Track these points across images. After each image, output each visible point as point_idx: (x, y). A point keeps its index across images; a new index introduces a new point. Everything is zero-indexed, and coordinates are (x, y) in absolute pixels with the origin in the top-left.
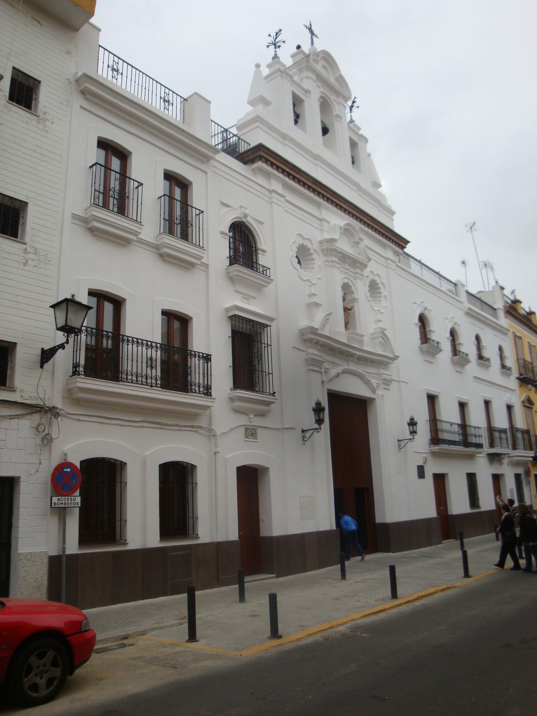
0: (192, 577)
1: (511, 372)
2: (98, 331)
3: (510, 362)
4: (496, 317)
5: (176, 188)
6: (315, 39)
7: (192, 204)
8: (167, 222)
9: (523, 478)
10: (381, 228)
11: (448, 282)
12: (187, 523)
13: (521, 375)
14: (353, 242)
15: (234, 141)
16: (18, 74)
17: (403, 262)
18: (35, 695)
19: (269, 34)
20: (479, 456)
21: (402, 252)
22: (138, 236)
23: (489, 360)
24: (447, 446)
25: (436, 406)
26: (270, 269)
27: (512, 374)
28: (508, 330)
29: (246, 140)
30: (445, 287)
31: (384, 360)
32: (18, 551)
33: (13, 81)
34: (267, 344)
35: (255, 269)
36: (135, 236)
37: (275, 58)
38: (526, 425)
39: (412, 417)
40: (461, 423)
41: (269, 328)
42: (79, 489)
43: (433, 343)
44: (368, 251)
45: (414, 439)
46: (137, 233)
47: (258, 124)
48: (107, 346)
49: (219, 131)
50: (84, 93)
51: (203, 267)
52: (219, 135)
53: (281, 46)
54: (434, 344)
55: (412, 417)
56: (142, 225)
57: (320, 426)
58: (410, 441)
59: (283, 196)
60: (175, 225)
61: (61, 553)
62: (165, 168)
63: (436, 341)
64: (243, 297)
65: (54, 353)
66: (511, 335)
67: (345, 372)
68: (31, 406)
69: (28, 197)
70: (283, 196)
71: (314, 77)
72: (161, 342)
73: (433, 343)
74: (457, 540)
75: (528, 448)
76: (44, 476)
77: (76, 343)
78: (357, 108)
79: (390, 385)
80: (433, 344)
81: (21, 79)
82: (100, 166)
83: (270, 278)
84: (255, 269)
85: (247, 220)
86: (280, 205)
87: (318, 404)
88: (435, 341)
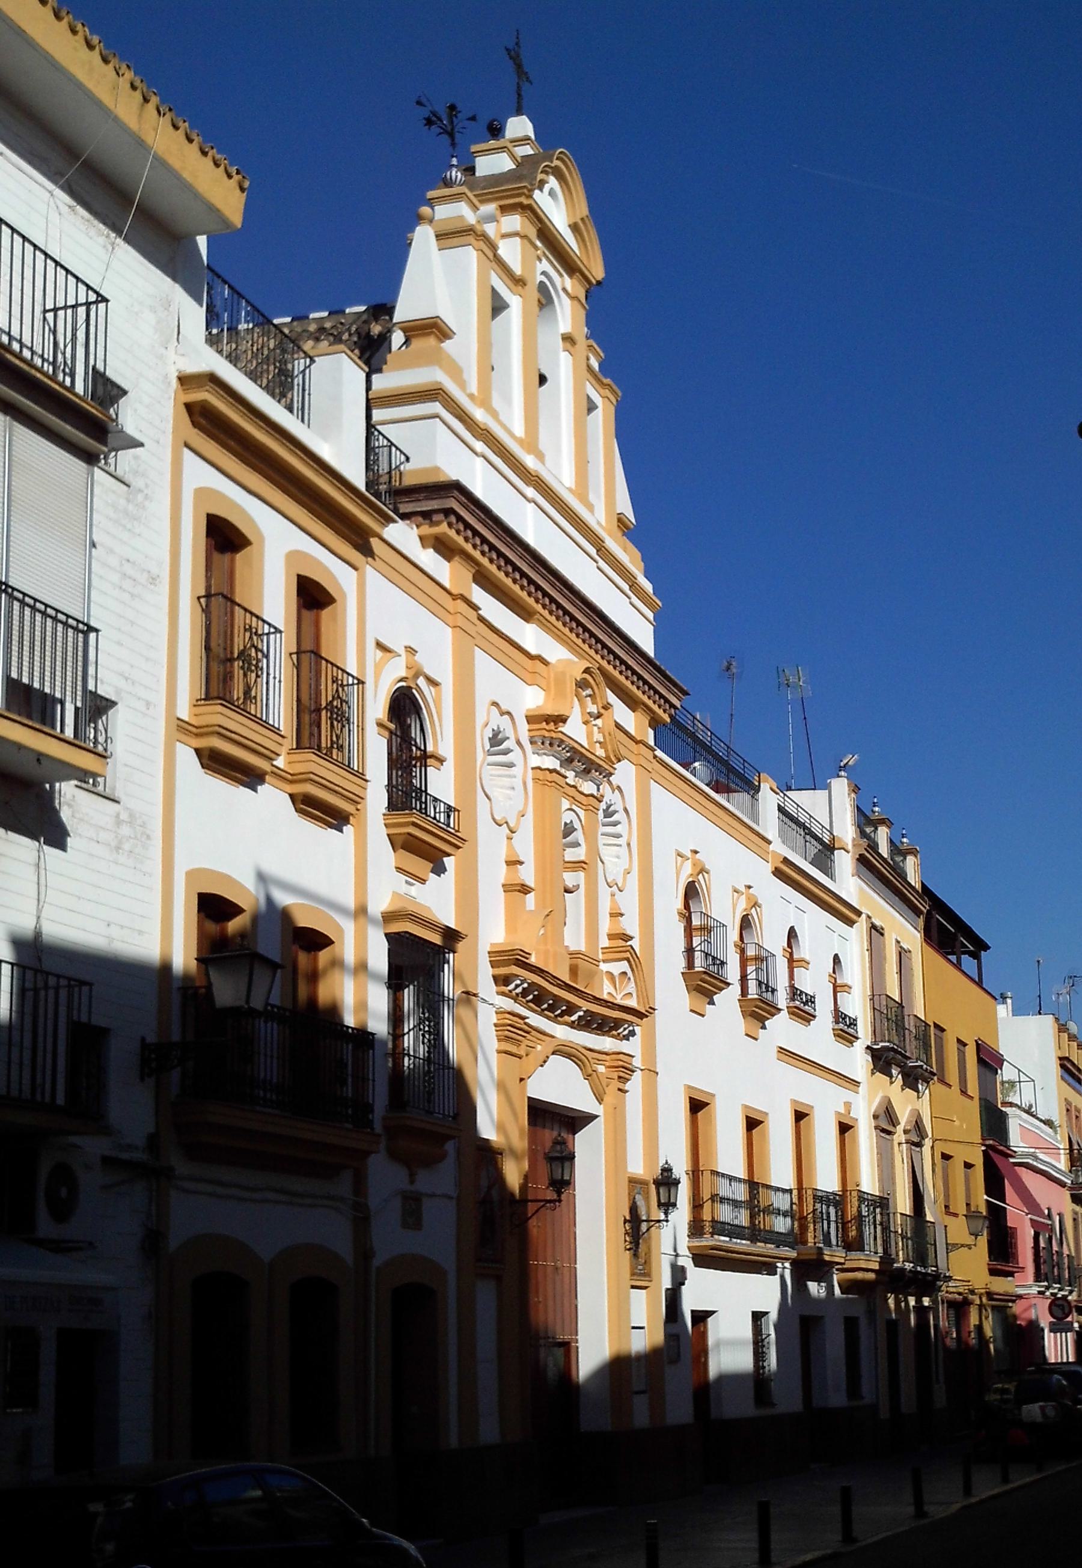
0: (325, 439)
1: (815, 1010)
2: (549, 1135)
3: (857, 1005)
4: (828, 871)
5: (82, 390)
6: (526, 86)
7: (345, 664)
8: (910, 1242)
9: (863, 1323)
10: (368, 1059)
11: (794, 826)
12: (68, 398)
13: (876, 1043)
14: (589, 713)
15: (341, 704)
16: (139, 122)
17: (269, 1038)
18: (1041, 1404)
19: (965, 1163)
20: (273, 982)
21: (651, 758)
22: (275, 763)
23: (813, 1002)
24: (727, 1239)
25: (493, 580)
26: (100, 633)
27: (857, 1038)
28: (859, 913)
29: (330, 659)
30: (408, 997)
31: (82, 436)
32: (166, 968)
33: (529, 1107)
34: (444, 1066)
35: (259, 383)
36: (435, 401)
37: (890, 1128)
38: (747, 1174)
39: (667, 1163)
40: (644, 1172)
41: (456, 813)
42: (608, 690)
43: (435, 808)
44: (620, 746)
45: (667, 1221)
46: (273, 756)
47: (436, 407)
48: (20, 1091)
49: (82, 299)
50: (1062, 1066)
51: (91, 519)
52: (411, 1033)
53: (426, 125)
54: (390, 447)
55: (667, 1163)
56: (366, 781)
57: (667, 1217)
58: (657, 1225)
59: (629, 598)
60: (909, 1235)
61: (242, 1003)
62: (302, 573)
63: (445, 803)
64: (603, 542)
65: (920, 1277)
66: (862, 924)
67: (437, 416)
68: (995, 1296)
69: (118, 691)
70: (629, 598)
71: (532, 233)
72: (440, 218)
73: (435, 808)
74: (559, 661)
75: (489, 136)
76: (348, 1126)
77: (361, 757)
78: (473, 123)
79: (628, 1080)
80: (432, 815)
81: (696, 1314)
82: (99, 692)
83: (681, 1169)
84: (259, 383)
85: (417, 685)
86: (179, 326)
87: (667, 1170)
88: (441, 801)
